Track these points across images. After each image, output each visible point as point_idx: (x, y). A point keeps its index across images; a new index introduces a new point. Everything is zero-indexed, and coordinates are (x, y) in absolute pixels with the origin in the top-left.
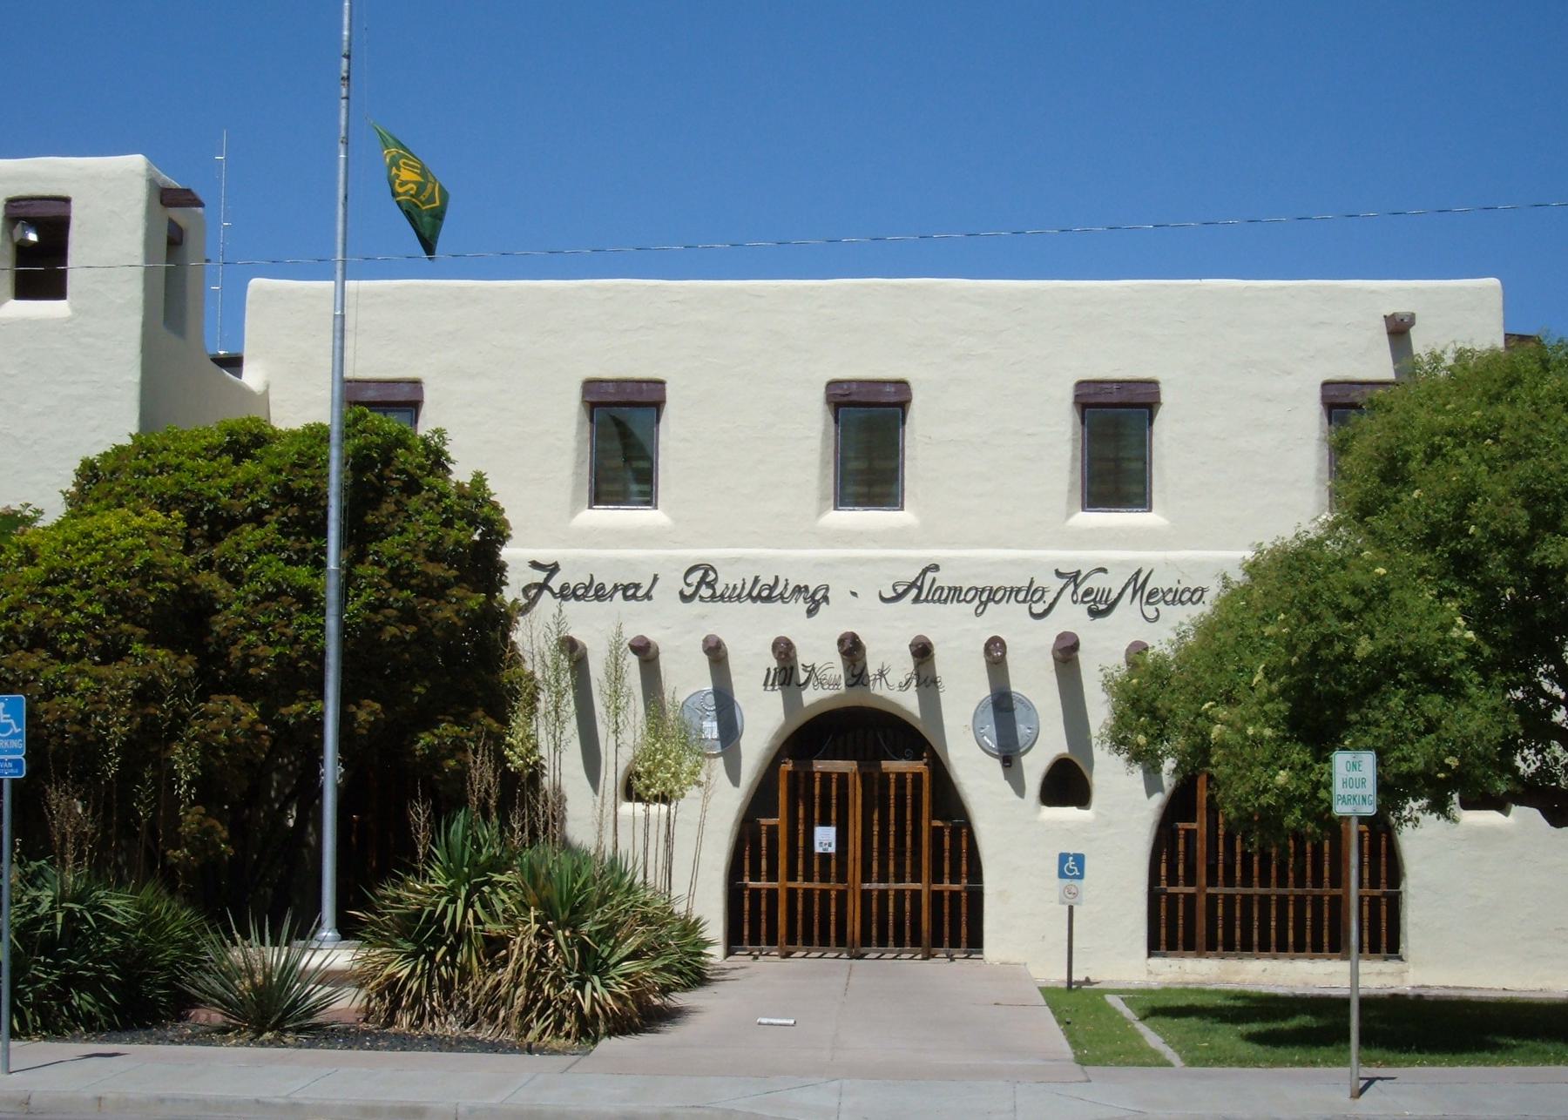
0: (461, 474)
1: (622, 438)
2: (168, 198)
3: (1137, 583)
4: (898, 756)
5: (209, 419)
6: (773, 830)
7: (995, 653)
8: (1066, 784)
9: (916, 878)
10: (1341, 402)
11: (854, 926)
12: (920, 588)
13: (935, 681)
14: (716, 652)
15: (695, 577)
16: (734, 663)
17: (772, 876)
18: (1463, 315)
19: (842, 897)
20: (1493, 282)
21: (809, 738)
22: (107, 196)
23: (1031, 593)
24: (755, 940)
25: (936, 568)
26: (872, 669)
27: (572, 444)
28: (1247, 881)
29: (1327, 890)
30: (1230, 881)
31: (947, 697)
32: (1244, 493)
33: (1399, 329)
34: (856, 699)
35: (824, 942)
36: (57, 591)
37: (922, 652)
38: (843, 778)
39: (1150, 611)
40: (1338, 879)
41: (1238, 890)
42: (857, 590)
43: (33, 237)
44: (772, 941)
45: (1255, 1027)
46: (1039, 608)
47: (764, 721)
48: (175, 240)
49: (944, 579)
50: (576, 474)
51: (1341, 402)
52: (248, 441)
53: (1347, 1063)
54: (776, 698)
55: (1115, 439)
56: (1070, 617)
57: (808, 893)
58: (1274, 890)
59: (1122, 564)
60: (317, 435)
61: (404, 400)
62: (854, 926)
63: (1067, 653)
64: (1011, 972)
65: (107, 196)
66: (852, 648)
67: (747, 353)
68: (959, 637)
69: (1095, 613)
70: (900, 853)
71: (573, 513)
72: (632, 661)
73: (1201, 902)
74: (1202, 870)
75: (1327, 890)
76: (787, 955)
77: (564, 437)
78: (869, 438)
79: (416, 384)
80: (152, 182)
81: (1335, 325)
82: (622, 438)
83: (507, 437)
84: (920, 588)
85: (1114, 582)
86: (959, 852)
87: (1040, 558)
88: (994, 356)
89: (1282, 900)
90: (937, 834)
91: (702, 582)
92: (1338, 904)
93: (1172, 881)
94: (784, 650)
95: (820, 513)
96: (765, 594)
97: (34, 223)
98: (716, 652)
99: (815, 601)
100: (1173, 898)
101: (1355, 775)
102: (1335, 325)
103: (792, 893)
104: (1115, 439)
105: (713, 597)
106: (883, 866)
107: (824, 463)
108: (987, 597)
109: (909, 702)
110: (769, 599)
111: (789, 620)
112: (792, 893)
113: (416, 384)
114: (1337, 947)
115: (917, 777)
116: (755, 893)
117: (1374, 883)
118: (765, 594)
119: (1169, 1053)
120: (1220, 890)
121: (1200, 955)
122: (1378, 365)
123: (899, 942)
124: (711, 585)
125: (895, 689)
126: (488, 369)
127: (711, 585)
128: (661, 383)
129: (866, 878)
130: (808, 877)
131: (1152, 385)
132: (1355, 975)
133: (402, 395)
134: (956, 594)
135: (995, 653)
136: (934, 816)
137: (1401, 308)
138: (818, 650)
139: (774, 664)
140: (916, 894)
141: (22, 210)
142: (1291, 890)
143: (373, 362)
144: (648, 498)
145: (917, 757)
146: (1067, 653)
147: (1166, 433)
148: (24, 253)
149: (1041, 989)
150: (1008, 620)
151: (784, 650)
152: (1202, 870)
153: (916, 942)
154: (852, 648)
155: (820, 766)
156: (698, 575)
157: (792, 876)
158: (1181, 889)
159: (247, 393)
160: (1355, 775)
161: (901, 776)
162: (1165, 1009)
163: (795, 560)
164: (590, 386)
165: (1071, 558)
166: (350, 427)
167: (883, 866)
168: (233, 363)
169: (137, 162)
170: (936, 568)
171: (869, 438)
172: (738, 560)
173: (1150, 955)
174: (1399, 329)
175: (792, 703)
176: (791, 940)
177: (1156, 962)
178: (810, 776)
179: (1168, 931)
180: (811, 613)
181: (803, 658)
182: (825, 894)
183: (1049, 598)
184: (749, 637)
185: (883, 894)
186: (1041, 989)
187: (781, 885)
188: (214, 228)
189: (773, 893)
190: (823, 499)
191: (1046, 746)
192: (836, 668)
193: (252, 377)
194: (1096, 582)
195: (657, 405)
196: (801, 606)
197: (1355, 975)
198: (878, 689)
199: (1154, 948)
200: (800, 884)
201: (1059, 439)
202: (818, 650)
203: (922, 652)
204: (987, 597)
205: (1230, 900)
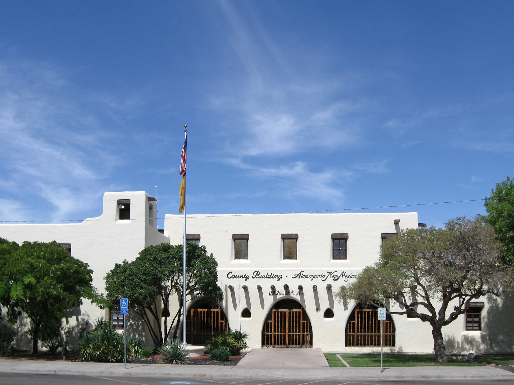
0: (208, 254)
1: (240, 245)
2: (150, 199)
3: (343, 274)
4: (296, 308)
5: (157, 243)
6: (271, 323)
7: (315, 288)
8: (329, 313)
9: (299, 332)
10: (384, 237)
11: (287, 342)
12: (300, 275)
13: (303, 294)
14: (259, 288)
15: (255, 274)
16: (250, 291)
17: (271, 332)
18: (410, 221)
19: (285, 335)
20: (416, 213)
21: (278, 305)
22: (138, 199)
23: (322, 276)
24: (268, 344)
25: (303, 271)
26: (291, 291)
27: (231, 247)
28: (365, 332)
29: (377, 333)
30: (361, 332)
31: (306, 297)
32: (365, 254)
33: (397, 223)
34: (288, 297)
35: (281, 344)
36: (131, 278)
37: (300, 288)
38: (285, 313)
39: (346, 280)
40: (379, 332)
41: (363, 334)
42: (288, 276)
43: (123, 207)
44: (271, 344)
45: (374, 359)
46: (323, 279)
47: (269, 301)
48: (151, 208)
49: (305, 274)
50: (232, 253)
51: (384, 237)
52: (166, 248)
53: (380, 366)
54: (272, 297)
55: (339, 245)
56: (330, 281)
57: (278, 335)
58: (367, 334)
59: (340, 270)
60: (181, 247)
61: (197, 238)
62: (287, 342)
63: (329, 288)
64: (318, 350)
65: (138, 199)
66: (286, 287)
67: (265, 229)
68: (307, 285)
69: (335, 280)
70: (375, 329)
71: (231, 261)
72: (229, 290)
73: (356, 336)
74: (356, 329)
75: (377, 333)
76: (274, 347)
77: (229, 246)
78: (290, 245)
79: (199, 235)
80: (146, 196)
81: (383, 222)
82: (240, 245)
83: (217, 246)
84: (300, 275)
85: (338, 274)
86: (308, 327)
87: (324, 270)
88: (315, 230)
89: (372, 336)
90: (303, 323)
91: (257, 275)
92: (379, 336)
93: (350, 332)
94: (273, 288)
95: (280, 260)
96: (269, 277)
97: (123, 204)
98: (259, 288)
99: (279, 278)
100: (350, 335)
101: (382, 312)
102: (383, 222)
103: (275, 335)
104: (339, 245)
105: (259, 278)
106: (293, 330)
107: (281, 250)
108: (313, 277)
109: (298, 298)
110: (270, 278)
111: (274, 282)
112: (275, 335)
113: (199, 235)
114: (379, 345)
115: (299, 312)
116: (268, 335)
117: (386, 332)
118: (269, 277)
119: (347, 365)
120: (359, 334)
121: (355, 346)
122: (393, 230)
123: (296, 344)
124: (258, 275)
125: (295, 295)
126: (214, 233)
127: (258, 275)
128: (248, 235)
129: (289, 332)
130: (278, 332)
131: (347, 235)
132: (382, 349)
133: (294, 236)
134: (307, 276)
135: (315, 288)
136: (221, 320)
137: (397, 219)
138: (280, 287)
139: (271, 290)
140: (299, 335)
141: (120, 202)
142: (295, 333)
143: (191, 231)
144: (345, 258)
145: (300, 308)
146: (329, 288)
147: (350, 243)
148: (121, 210)
149: (324, 354)
150: (317, 282)
151: (273, 288)
152: (356, 329)
153: (299, 344)
154: (286, 287)
155: (280, 310)
156: (256, 273)
157: (275, 331)
158: (352, 334)
159: (165, 237)
160: (382, 312)
161: (296, 312)
162: (346, 356)
163: (275, 270)
164: (234, 235)
165: (330, 269)
166: (188, 244)
167: (293, 330)
168: (162, 231)
169: (143, 192)
170: (303, 271)
171: (290, 245)
172: (264, 270)
173: (262, 347)
174: (397, 223)
175: (274, 298)
176: (275, 344)
177: (347, 348)
178: (211, 312)
179: (349, 342)
180: (278, 280)
181: (277, 289)
182: (281, 335)
183: (326, 277)
184: (266, 285)
185: (293, 335)
186: (324, 354)
187: (273, 333)
188: (156, 204)
189: (271, 335)
190: (281, 257)
191: (325, 305)
192: (283, 291)
193: (166, 234)
194: (335, 274)
195: (247, 239)
196: (244, 279)
197: (382, 349)
198: (292, 295)
199: (346, 345)
200: (276, 333)
201: (328, 245)
202: (280, 287)
203: (300, 288)
204: (313, 277)
205: (361, 336)
